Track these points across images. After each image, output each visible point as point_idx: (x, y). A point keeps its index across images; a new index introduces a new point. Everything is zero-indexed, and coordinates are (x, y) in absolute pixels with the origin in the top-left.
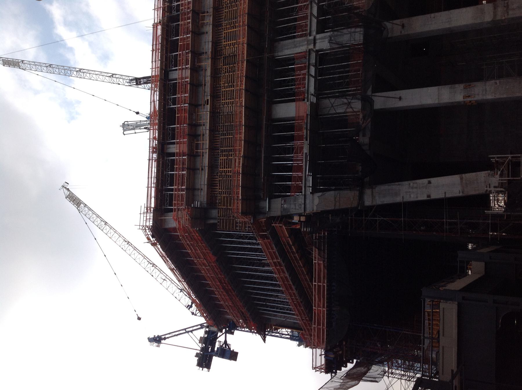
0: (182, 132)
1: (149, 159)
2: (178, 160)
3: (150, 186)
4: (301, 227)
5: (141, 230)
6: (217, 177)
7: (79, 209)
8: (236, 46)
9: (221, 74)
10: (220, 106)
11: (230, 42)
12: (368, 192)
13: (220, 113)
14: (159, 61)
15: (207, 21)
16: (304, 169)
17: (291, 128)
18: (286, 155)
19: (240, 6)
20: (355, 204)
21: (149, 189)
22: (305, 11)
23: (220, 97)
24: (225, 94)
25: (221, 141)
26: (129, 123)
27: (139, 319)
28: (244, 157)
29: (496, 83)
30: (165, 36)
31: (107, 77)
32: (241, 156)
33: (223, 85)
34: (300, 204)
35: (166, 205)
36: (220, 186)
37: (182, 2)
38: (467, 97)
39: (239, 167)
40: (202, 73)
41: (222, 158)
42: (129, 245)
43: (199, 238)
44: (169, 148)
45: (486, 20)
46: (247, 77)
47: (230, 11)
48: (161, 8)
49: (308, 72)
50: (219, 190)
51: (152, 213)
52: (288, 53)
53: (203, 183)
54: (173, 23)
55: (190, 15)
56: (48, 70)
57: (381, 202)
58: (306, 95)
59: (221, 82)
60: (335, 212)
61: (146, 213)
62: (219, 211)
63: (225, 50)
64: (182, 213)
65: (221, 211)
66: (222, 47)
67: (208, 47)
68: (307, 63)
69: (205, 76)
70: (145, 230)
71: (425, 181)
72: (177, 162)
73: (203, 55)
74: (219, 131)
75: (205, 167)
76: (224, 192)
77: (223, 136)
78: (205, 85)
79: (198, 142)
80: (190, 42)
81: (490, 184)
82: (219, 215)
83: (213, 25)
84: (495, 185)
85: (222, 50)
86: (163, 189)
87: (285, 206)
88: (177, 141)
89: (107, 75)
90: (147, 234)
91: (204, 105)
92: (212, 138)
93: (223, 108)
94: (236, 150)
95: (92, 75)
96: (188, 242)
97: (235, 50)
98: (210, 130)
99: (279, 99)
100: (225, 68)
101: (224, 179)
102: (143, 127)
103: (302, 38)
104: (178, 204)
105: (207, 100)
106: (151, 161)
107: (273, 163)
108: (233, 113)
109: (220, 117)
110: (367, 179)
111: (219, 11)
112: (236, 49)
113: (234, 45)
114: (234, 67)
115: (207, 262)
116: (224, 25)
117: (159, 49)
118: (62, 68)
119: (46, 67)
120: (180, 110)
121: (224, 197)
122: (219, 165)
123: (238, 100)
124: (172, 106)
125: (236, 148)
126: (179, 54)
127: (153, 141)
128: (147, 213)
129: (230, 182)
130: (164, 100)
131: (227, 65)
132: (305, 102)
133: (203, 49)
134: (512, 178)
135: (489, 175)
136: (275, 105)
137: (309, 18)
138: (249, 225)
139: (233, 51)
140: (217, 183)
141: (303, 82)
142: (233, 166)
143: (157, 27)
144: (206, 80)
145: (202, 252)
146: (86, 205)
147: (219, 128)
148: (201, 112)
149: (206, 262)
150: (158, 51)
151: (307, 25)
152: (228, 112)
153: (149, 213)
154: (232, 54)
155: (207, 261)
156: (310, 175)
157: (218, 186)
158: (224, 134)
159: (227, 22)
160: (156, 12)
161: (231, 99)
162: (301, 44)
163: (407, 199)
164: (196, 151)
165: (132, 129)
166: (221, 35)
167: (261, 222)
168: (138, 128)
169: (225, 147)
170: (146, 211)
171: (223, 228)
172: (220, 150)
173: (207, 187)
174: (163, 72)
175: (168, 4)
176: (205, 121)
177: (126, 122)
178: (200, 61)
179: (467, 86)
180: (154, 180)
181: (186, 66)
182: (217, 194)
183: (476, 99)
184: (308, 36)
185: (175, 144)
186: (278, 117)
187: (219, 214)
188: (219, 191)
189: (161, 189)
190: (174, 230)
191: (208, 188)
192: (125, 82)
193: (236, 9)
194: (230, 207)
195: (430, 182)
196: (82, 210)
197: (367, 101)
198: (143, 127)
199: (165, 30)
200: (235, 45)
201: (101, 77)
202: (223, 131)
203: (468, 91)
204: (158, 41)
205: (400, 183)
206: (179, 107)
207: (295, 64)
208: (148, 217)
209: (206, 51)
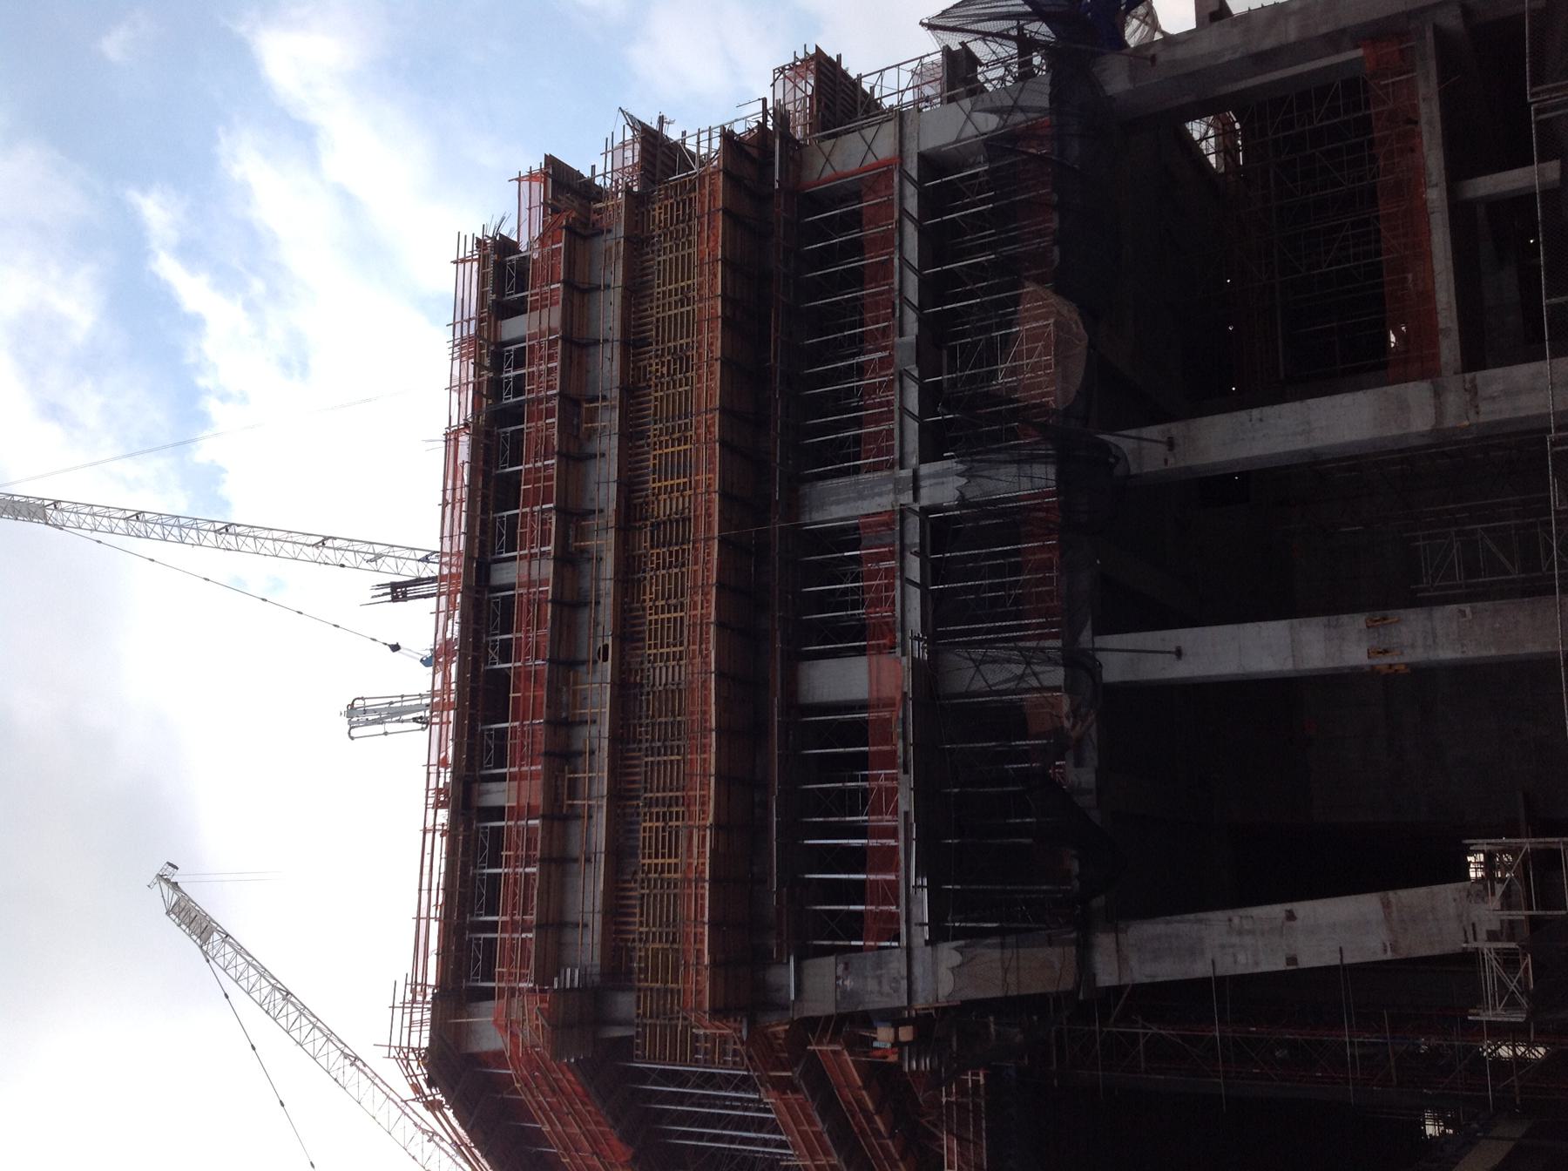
0: (520, 892)
1: (425, 828)
2: (515, 830)
3: (424, 914)
4: (901, 1057)
5: (394, 1060)
6: (633, 885)
7: (205, 948)
8: (688, 492)
9: (644, 572)
10: (643, 666)
11: (669, 482)
12: (1104, 942)
13: (642, 686)
14: (462, 536)
15: (603, 424)
16: (902, 864)
17: (859, 732)
18: (845, 816)
19: (698, 383)
20: (1068, 983)
21: (423, 923)
22: (884, 394)
23: (643, 639)
24: (656, 629)
25: (646, 772)
26: (368, 702)
27: (396, 648)
28: (718, 826)
29: (1463, 613)
30: (481, 463)
31: (309, 546)
32: (708, 825)
33: (651, 604)
34: (894, 978)
35: (478, 910)
36: (642, 915)
37: (530, 370)
38: (1381, 653)
39: (701, 854)
40: (588, 568)
41: (648, 824)
42: (358, 1068)
43: (574, 1086)
44: (488, 792)
45: (1414, 429)
46: (721, 586)
47: (668, 396)
48: (471, 386)
49: (902, 569)
50: (641, 929)
51: (429, 1006)
52: (842, 514)
53: (588, 907)
54: (506, 427)
55: (555, 402)
56: (130, 530)
57: (1147, 976)
58: (899, 635)
59: (644, 594)
60: (1006, 1007)
61: (410, 1005)
62: (639, 997)
63: (656, 503)
64: (523, 1007)
65: (645, 997)
66: (647, 496)
67: (604, 491)
68: (898, 543)
69: (598, 579)
70: (405, 1062)
71: (1277, 910)
72: (509, 839)
73: (591, 517)
74: (641, 741)
75: (598, 855)
76: (654, 934)
77: (652, 756)
78: (598, 603)
79: (576, 776)
80: (555, 483)
81: (1473, 925)
82: (641, 1011)
83: (621, 435)
84: (1489, 929)
85: (647, 504)
86: (464, 923)
87: (847, 983)
88: (512, 770)
89: (308, 542)
90: (411, 1073)
91: (595, 662)
92: (619, 762)
93: (652, 670)
94: (693, 800)
95: (262, 541)
96: (541, 1098)
97: (687, 505)
98: (614, 739)
99: (817, 648)
100: (658, 554)
101: (655, 891)
102: (411, 716)
103: (879, 474)
104: (510, 974)
105: (604, 646)
106: (429, 836)
107: (806, 842)
108: (681, 687)
109: (643, 698)
110: (1099, 902)
111: (639, 397)
112: (690, 502)
113: (681, 489)
114: (684, 550)
115: (602, 1163)
116: (651, 434)
117: (461, 501)
118: (172, 522)
119: (124, 519)
120: (524, 675)
121: (655, 953)
122: (638, 846)
123: (697, 647)
124: (497, 666)
125: (691, 793)
126: (522, 513)
127: (438, 773)
128: (414, 1005)
129: (675, 902)
130: (476, 647)
131: (664, 547)
132: (898, 658)
133: (592, 500)
134: (1541, 913)
135: (1468, 896)
136: (808, 663)
137: (897, 416)
138: (735, 1047)
139: (680, 507)
140: (634, 906)
141: (888, 594)
142: (682, 849)
143: (456, 439)
144: (601, 588)
145: (587, 1133)
146: (227, 935)
147: (640, 732)
148: (585, 684)
149: (599, 1164)
150: (461, 506)
151: (890, 432)
152: (666, 684)
153: (421, 1005)
154: (677, 514)
155: (602, 1159)
156: (922, 887)
157: (638, 916)
158: (656, 750)
159: (661, 425)
160: (455, 395)
161: (675, 646)
162: (876, 490)
163: (1227, 967)
164: (570, 802)
165: (375, 722)
166: (643, 461)
167: (775, 1035)
168: (394, 719)
169: (658, 791)
170: (409, 997)
171: (652, 1056)
172: (642, 798)
173: (601, 919)
174: (475, 565)
175: (491, 375)
176: (597, 710)
177: (358, 699)
178: (582, 534)
179: (1376, 621)
180: (438, 897)
181: (543, 549)
182: (634, 940)
183: (1406, 659)
184: (897, 467)
185: (505, 781)
186: (816, 701)
187: (638, 1008)
188: (641, 933)
189: (458, 924)
190: (498, 1057)
191: (604, 924)
192: (359, 559)
193: (686, 391)
194: (674, 985)
195: (1291, 916)
196: (215, 951)
197: (1080, 664)
198: (411, 716)
199: (468, 689)
200: (685, 490)
201: (288, 546)
202: (653, 740)
203: (1379, 635)
204: (459, 475)
205: (1202, 915)
206: (526, 554)
207: (864, 543)
208: (417, 1017)
209: (601, 506)
